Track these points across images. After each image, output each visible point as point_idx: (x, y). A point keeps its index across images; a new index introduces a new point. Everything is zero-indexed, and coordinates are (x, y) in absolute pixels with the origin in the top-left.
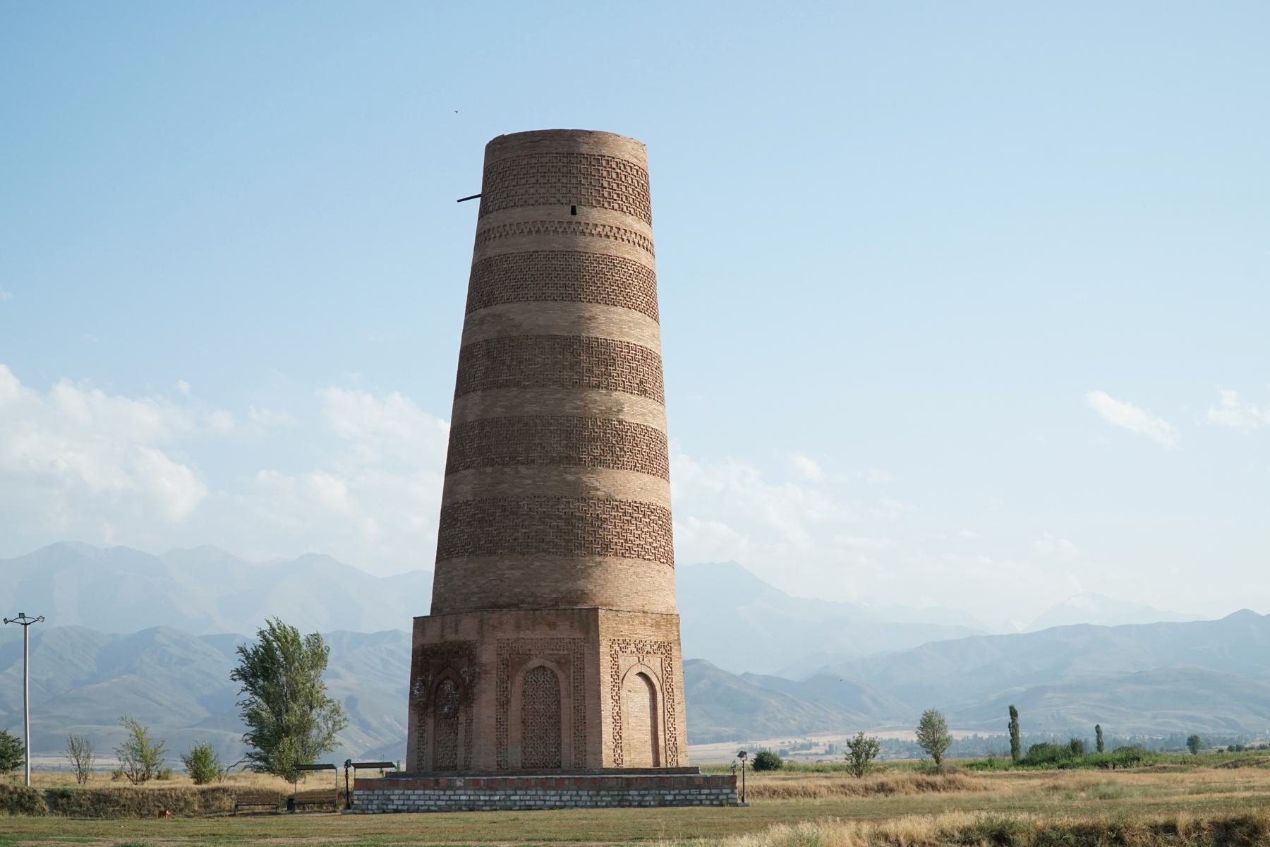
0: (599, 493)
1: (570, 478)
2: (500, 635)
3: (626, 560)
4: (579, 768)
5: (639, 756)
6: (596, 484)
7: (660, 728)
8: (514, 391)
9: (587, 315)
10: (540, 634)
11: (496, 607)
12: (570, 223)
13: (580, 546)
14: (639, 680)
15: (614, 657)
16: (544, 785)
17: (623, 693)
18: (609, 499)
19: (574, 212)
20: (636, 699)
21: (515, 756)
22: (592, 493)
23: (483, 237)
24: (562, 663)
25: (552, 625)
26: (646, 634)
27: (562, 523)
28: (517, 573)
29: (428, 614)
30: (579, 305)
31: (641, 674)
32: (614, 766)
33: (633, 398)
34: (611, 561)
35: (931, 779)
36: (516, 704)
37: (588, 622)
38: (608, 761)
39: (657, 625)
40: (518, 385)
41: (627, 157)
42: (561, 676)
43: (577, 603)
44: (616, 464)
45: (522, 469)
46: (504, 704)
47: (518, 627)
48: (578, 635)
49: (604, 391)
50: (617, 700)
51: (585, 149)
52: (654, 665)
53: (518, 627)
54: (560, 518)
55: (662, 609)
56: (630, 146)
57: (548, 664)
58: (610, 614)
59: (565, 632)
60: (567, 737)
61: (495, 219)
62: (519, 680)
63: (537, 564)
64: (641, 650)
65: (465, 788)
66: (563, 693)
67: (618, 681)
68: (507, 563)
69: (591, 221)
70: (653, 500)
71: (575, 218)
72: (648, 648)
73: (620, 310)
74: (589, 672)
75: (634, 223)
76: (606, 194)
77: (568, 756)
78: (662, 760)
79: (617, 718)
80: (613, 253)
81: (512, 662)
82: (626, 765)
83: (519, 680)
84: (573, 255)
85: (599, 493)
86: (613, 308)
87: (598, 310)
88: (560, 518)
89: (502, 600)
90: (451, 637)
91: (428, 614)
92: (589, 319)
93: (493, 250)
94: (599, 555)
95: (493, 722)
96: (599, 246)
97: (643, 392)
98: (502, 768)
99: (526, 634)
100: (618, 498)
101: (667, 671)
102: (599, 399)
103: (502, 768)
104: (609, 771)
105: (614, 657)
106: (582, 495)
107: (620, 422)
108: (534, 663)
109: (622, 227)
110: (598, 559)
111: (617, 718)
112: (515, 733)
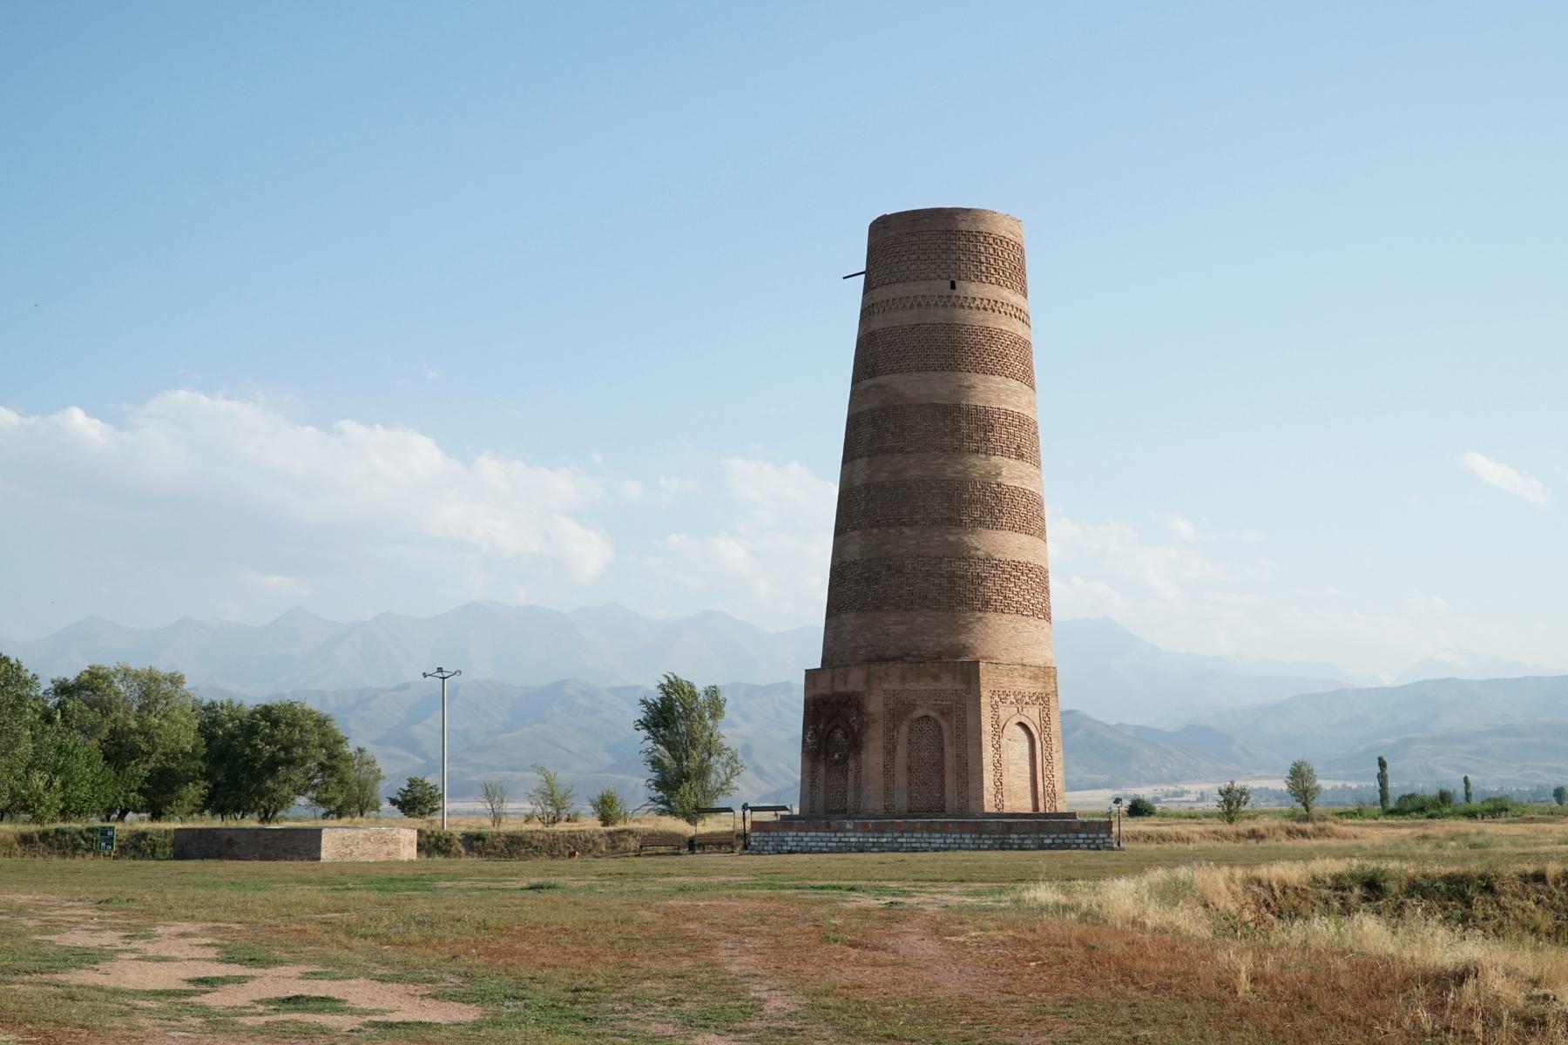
1: (951, 538)
2: (886, 686)
4: (963, 812)
5: (1019, 801)
8: (898, 457)
10: (920, 686)
11: (883, 660)
13: (961, 603)
15: (995, 708)
16: (929, 828)
18: (989, 558)
19: (953, 286)
20: (1016, 747)
21: (901, 801)
23: (867, 313)
25: (936, 678)
26: (1025, 685)
27: (944, 582)
28: (902, 628)
29: (819, 666)
30: (959, 374)
32: (995, 810)
34: (991, 617)
36: (902, 751)
37: (969, 674)
38: (989, 807)
39: (1035, 678)
40: (901, 450)
41: (1003, 233)
44: (996, 525)
45: (906, 530)
46: (890, 751)
47: (903, 679)
48: (963, 687)
50: (997, 749)
51: (963, 226)
52: (1032, 715)
53: (903, 679)
55: (1040, 662)
57: (932, 714)
58: (991, 667)
59: (947, 683)
60: (950, 782)
62: (904, 729)
63: (921, 620)
64: (1020, 701)
65: (855, 830)
67: (999, 730)
69: (970, 294)
71: (955, 293)
73: (997, 378)
74: (970, 721)
77: (951, 801)
80: (991, 324)
81: (898, 712)
82: (1006, 810)
83: (904, 729)
84: (952, 327)
87: (977, 379)
90: (841, 688)
91: (819, 666)
93: (877, 324)
96: (977, 319)
97: (1021, 456)
98: (889, 812)
99: (912, 686)
101: (1046, 721)
102: (978, 464)
103: (889, 812)
105: (995, 708)
106: (963, 554)
107: (999, 485)
108: (919, 713)
110: (979, 615)
111: (998, 765)
112: (901, 780)
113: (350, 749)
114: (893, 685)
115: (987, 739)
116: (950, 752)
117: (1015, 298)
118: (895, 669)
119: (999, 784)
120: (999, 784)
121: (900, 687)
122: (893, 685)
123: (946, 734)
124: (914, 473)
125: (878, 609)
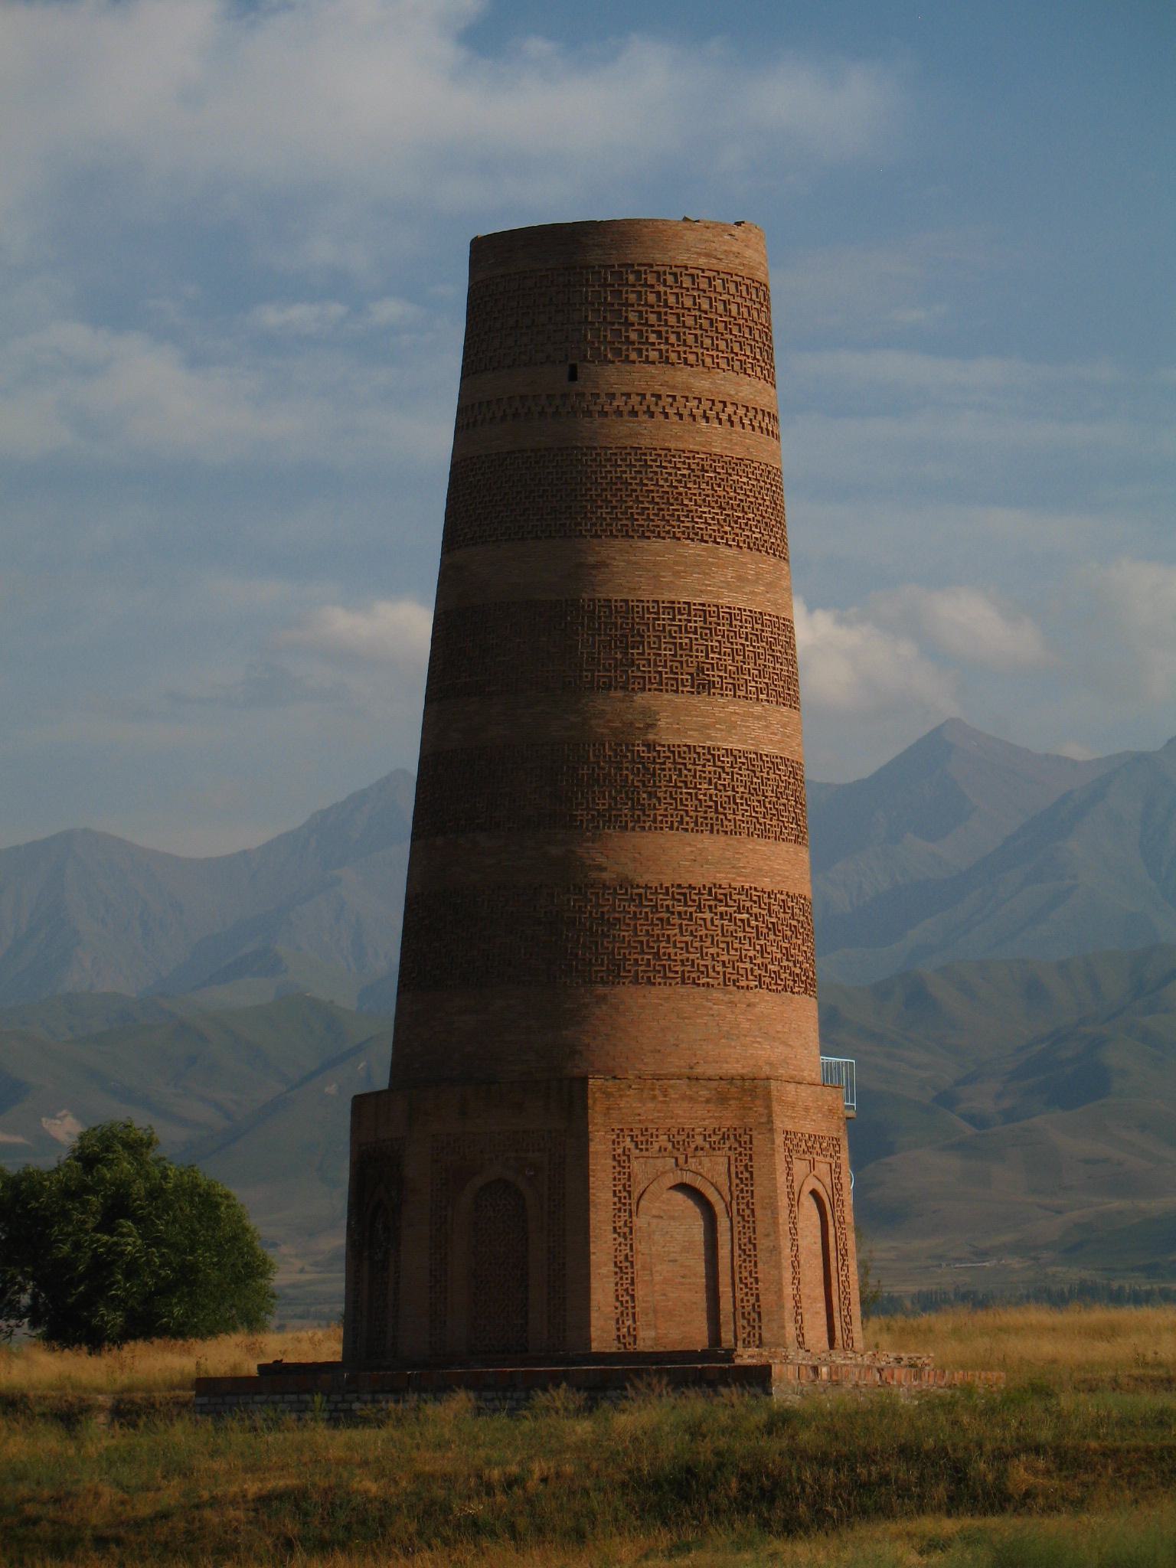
0: (605, 875)
3: (654, 990)
5: (674, 1321)
6: (601, 860)
7: (724, 1279)
9: (591, 560)
12: (565, 396)
14: (679, 1196)
17: (639, 1222)
18: (626, 883)
19: (573, 376)
22: (594, 875)
26: (697, 1115)
29: (338, 1359)
31: (682, 1187)
33: (679, 699)
34: (629, 995)
37: (569, 1101)
39: (723, 1099)
41: (682, 258)
44: (634, 531)
46: (1017, 1330)
49: (620, 694)
50: (626, 1233)
52: (713, 1171)
55: (734, 1068)
56: (690, 236)
64: (681, 1144)
67: (627, 1201)
72: (699, 1140)
73: (657, 545)
75: (747, 389)
76: (634, 336)
78: (727, 1336)
79: (624, 1267)
80: (645, 442)
82: (642, 1346)
85: (605, 875)
86: (643, 543)
92: (595, 567)
94: (604, 983)
96: (620, 432)
97: (703, 686)
100: (642, 881)
104: (602, 1358)
105: (621, 1161)
107: (650, 746)
109: (664, 391)
110: (601, 990)
111: (624, 1267)
117: (747, 389)
119: (626, 1296)
120: (626, 1296)
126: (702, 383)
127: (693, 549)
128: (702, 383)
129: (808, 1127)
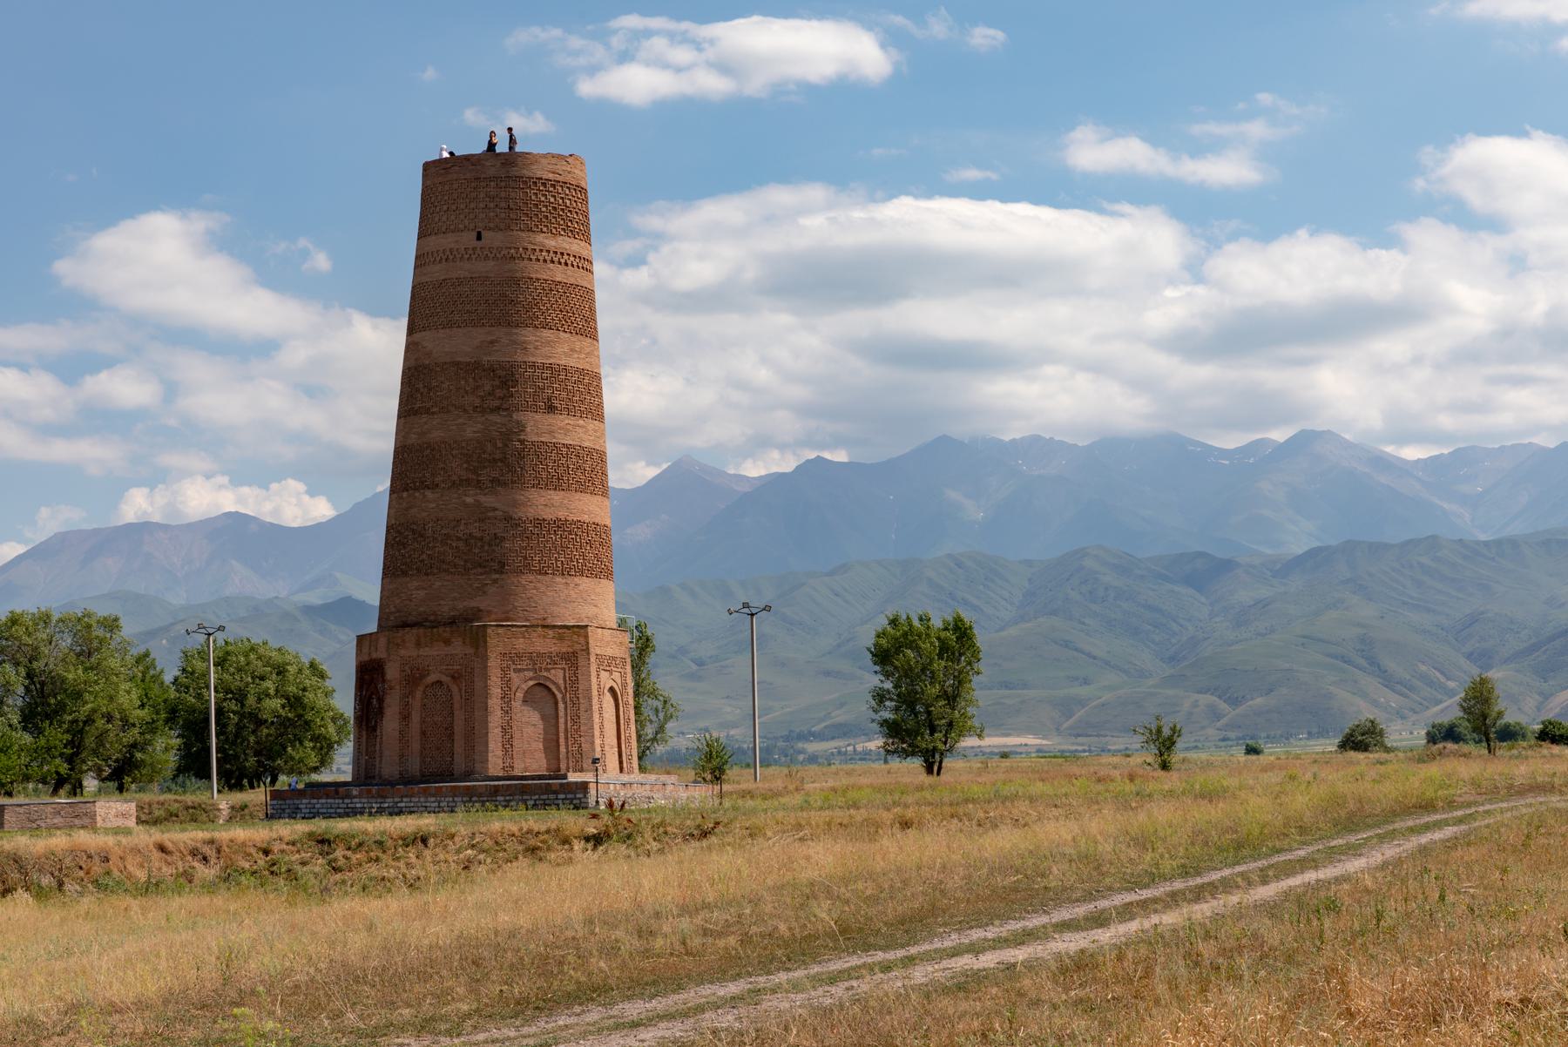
2: (402, 652)
5: (531, 761)
8: (425, 418)
11: (405, 625)
16: (426, 792)
18: (539, 522)
19: (479, 237)
23: (421, 260)
24: (455, 678)
25: (447, 642)
27: (461, 544)
28: (422, 593)
35: (852, 780)
36: (416, 717)
40: (428, 411)
42: (455, 689)
43: (472, 621)
45: (429, 493)
46: (405, 717)
47: (418, 645)
48: (472, 651)
53: (418, 645)
54: (459, 539)
57: (445, 679)
59: (458, 648)
61: (435, 242)
62: (419, 694)
63: (438, 583)
65: (360, 796)
66: (456, 706)
68: (415, 584)
70: (562, 514)
75: (575, 246)
82: (517, 772)
83: (419, 694)
87: (528, 335)
88: (459, 539)
89: (412, 619)
90: (374, 656)
93: (437, 272)
95: (397, 734)
97: (551, 409)
107: (522, 442)
113: (460, 808)
114: (409, 651)
115: (494, 703)
116: (459, 716)
117: (575, 246)
118: (410, 635)
121: (415, 654)
122: (409, 651)
123: (456, 697)
124: (436, 435)
125: (405, 573)
126: (551, 243)
127: (546, 333)
128: (551, 243)
129: (609, 652)
